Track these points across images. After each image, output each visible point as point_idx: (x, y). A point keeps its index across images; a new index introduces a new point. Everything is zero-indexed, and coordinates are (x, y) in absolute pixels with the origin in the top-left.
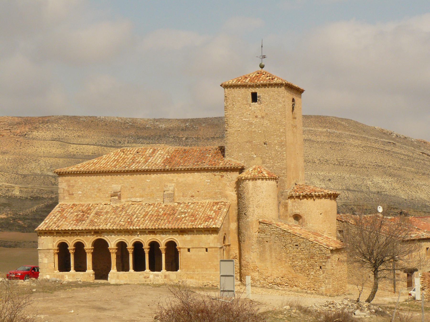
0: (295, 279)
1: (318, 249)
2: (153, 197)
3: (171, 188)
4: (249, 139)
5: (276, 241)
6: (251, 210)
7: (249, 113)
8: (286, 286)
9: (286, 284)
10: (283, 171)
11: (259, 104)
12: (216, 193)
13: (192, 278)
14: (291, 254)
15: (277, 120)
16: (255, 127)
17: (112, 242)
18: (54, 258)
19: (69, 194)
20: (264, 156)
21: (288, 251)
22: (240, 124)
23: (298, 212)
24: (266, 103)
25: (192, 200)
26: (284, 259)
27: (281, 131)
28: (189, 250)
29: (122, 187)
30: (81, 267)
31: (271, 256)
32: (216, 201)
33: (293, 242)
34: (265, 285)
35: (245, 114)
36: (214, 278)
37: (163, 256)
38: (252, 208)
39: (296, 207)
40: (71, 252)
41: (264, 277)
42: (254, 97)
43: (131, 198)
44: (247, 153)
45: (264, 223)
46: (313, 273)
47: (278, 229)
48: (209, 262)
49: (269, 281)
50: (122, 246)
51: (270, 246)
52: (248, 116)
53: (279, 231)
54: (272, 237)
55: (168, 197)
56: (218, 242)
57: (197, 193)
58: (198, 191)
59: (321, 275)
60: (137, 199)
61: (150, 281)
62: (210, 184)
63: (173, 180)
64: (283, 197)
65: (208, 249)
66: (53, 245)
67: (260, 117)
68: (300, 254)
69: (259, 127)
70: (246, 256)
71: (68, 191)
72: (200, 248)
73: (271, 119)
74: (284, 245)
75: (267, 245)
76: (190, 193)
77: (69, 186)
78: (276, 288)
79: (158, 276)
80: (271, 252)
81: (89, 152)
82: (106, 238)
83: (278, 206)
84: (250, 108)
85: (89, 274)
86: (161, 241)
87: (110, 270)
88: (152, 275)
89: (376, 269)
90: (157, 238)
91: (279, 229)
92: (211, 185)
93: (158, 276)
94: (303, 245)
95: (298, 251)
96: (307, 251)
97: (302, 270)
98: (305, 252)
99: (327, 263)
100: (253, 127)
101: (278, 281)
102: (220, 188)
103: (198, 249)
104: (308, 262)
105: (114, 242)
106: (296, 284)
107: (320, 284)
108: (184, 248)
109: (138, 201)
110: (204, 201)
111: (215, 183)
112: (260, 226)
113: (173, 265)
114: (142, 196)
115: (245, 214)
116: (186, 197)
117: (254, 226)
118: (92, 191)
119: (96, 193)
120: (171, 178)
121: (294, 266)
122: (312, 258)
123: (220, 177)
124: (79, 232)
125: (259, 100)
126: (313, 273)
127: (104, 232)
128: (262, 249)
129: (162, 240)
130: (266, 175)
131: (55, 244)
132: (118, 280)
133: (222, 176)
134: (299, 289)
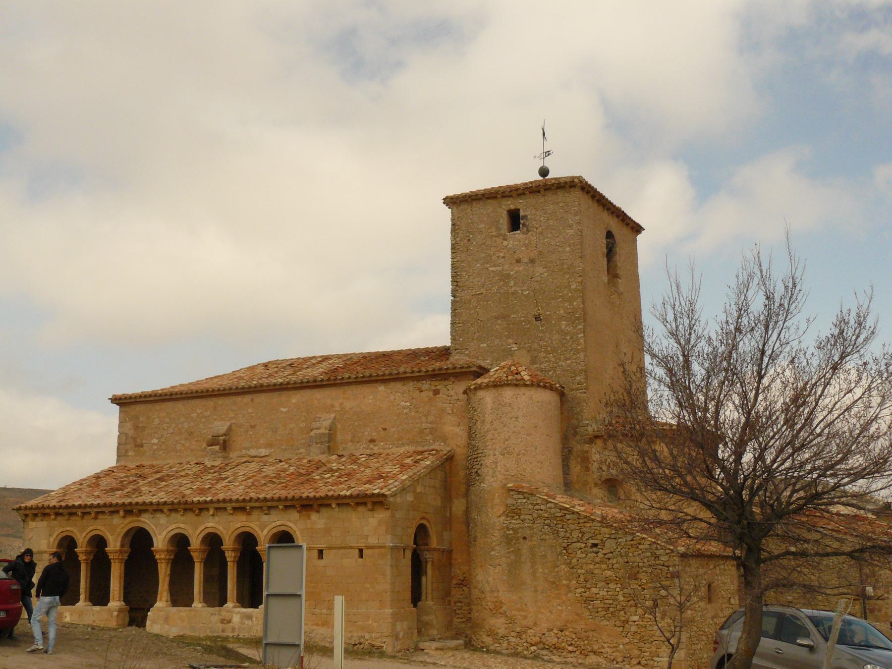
0: (591, 634)
1: (649, 554)
2: (292, 445)
3: (327, 423)
4: (502, 310)
5: (544, 537)
6: (488, 461)
7: (502, 255)
8: (571, 652)
9: (570, 648)
10: (578, 378)
11: (524, 233)
12: (421, 432)
14: (581, 568)
15: (563, 264)
16: (515, 285)
17: (161, 533)
19: (136, 446)
20: (535, 346)
21: (574, 561)
22: (483, 280)
24: (540, 229)
25: (372, 449)
26: (565, 582)
27: (573, 287)
28: (321, 553)
29: (233, 426)
30: (100, 597)
32: (420, 449)
33: (586, 536)
34: (520, 649)
35: (493, 257)
38: (492, 458)
40: (82, 557)
41: (518, 630)
42: (515, 221)
43: (248, 449)
44: (497, 341)
45: (519, 493)
46: (636, 618)
47: (549, 505)
48: (367, 585)
49: (529, 640)
50: (180, 542)
51: (532, 549)
52: (501, 260)
53: (553, 511)
54: (535, 526)
55: (317, 443)
57: (382, 433)
58: (385, 429)
60: (260, 450)
61: (233, 630)
62: (410, 411)
64: (578, 437)
65: (364, 552)
66: (49, 542)
67: (526, 260)
68: (604, 566)
69: (523, 283)
70: (480, 577)
71: (134, 439)
72: (345, 548)
73: (551, 262)
74: (565, 545)
75: (525, 547)
77: (136, 428)
78: (546, 658)
79: (249, 617)
81: (215, 408)
82: (147, 522)
84: (505, 243)
85: (110, 612)
86: (260, 532)
87: (155, 602)
88: (238, 616)
89: (754, 550)
90: (252, 525)
93: (249, 617)
95: (597, 560)
96: (620, 559)
98: (615, 561)
100: (512, 283)
101: (551, 639)
103: (342, 551)
104: (622, 588)
105: (164, 534)
106: (596, 647)
107: (654, 649)
109: (262, 455)
110: (394, 450)
111: (421, 410)
112: (510, 501)
114: (269, 445)
116: (358, 442)
117: (497, 501)
118: (177, 438)
119: (183, 442)
120: (329, 402)
121: (588, 601)
122: (634, 576)
123: (431, 394)
124: (97, 513)
125: (524, 225)
126: (636, 618)
127: (146, 511)
128: (513, 557)
130: (527, 378)
131: (52, 540)
132: (167, 627)
133: (436, 392)
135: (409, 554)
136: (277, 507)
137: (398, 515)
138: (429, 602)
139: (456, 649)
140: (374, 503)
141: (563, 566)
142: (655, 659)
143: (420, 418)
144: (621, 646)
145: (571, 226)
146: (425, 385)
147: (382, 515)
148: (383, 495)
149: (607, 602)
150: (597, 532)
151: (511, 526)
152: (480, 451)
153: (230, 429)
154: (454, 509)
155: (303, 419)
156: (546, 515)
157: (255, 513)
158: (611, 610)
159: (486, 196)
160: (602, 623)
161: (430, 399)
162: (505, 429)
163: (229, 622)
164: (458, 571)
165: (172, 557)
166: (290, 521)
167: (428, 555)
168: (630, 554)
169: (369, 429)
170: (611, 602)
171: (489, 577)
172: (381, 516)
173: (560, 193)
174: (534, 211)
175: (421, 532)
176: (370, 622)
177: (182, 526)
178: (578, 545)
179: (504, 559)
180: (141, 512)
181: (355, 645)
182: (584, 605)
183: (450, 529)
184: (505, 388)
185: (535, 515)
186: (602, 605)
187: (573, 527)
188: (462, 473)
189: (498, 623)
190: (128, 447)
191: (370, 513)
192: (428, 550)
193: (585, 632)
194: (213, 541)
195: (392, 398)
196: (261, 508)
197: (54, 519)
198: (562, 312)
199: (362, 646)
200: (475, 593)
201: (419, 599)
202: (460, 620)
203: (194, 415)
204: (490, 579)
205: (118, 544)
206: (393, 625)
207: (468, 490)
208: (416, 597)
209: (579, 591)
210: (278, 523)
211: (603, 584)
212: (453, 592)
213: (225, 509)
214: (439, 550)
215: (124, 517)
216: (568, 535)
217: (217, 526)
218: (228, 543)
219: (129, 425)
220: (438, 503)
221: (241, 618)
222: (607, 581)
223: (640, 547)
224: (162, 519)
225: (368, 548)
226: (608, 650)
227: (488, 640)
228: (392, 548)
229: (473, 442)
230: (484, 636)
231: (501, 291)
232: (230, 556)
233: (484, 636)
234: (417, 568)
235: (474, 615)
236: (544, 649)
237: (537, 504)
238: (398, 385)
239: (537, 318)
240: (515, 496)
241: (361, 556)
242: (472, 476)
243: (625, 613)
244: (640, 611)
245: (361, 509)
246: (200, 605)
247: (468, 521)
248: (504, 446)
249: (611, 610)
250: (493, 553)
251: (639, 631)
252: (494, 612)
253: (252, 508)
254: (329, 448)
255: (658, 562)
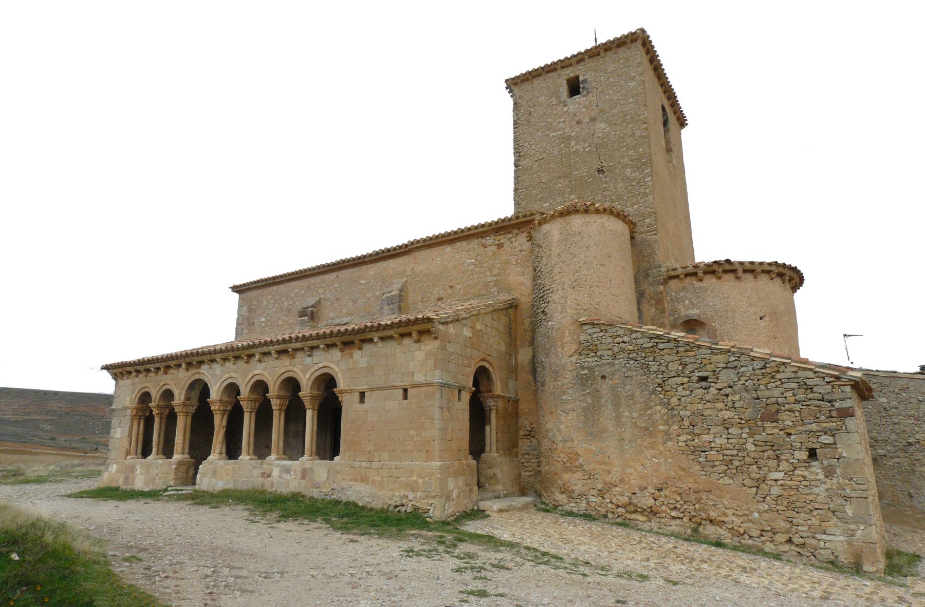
1: (794, 385)
3: (398, 286)
5: (629, 373)
6: (556, 297)
8: (674, 518)
9: (674, 514)
10: (647, 221)
12: (486, 285)
13: (364, 480)
15: (625, 116)
16: (577, 144)
18: (132, 426)
21: (674, 400)
23: (694, 313)
26: (661, 427)
31: (618, 419)
33: (690, 368)
36: (420, 481)
37: (309, 413)
38: (560, 292)
39: (687, 302)
41: (599, 487)
45: (593, 325)
46: (780, 475)
47: (633, 336)
48: (412, 432)
49: (614, 500)
50: (232, 389)
51: (613, 389)
52: (562, 125)
53: (639, 342)
54: (617, 362)
56: (435, 367)
57: (449, 291)
58: (451, 287)
59: (819, 484)
61: (272, 484)
63: (405, 271)
64: (651, 279)
67: (587, 120)
68: (720, 405)
70: (549, 426)
71: (248, 319)
73: (613, 116)
74: (659, 381)
75: (604, 388)
76: (437, 292)
79: (287, 470)
80: (617, 406)
83: (639, 303)
84: (565, 109)
86: (302, 376)
90: (295, 369)
91: (639, 335)
92: (478, 269)
93: (287, 470)
94: (726, 377)
95: (708, 397)
96: (745, 394)
97: (732, 464)
98: (737, 397)
99: (842, 437)
100: (573, 143)
102: (496, 271)
104: (751, 435)
105: (218, 384)
106: (713, 514)
107: (815, 521)
108: (352, 391)
113: (330, 446)
114: (348, 315)
115: (543, 312)
118: (279, 315)
122: (773, 417)
123: (495, 248)
125: (584, 88)
126: (780, 475)
128: (589, 400)
129: (306, 370)
133: (500, 246)
134: (722, 531)
135: (466, 397)
136: (317, 347)
137: (450, 348)
138: (492, 453)
139: (525, 507)
140: (421, 333)
141: (659, 408)
142: (818, 536)
143: (485, 272)
144: (756, 515)
145: (633, 79)
146: (489, 240)
147: (429, 345)
148: (429, 320)
149: (728, 452)
150: (705, 362)
151: (586, 365)
152: (546, 288)
153: (319, 302)
154: (519, 358)
155: (379, 288)
156: (631, 348)
157: (299, 355)
158: (736, 463)
159: (546, 69)
160: (721, 481)
161: (494, 254)
162: (575, 260)
163: (269, 476)
164: (525, 422)
165: (229, 408)
166: (332, 362)
167: (491, 403)
168: (762, 387)
169: (437, 289)
170: (735, 452)
171: (564, 426)
172: (429, 347)
173: (621, 51)
174: (593, 74)
175: (482, 376)
176: (414, 478)
177: (234, 375)
178: (679, 380)
179: (578, 403)
180: (201, 363)
181: (396, 507)
182: (691, 457)
183: (516, 379)
184: (573, 216)
185: (616, 349)
186: (721, 457)
187: (668, 358)
188: (527, 322)
189: (576, 481)
190: (244, 326)
191: (417, 345)
192: (492, 397)
193: (695, 492)
194: (260, 387)
195: (458, 257)
196: (302, 349)
197: (137, 376)
198: (626, 160)
199: (404, 509)
200: (546, 443)
201: (483, 450)
202: (528, 474)
203: (292, 295)
204: (562, 427)
205: (183, 397)
206: (443, 483)
207: (533, 338)
208: (477, 447)
209: (683, 438)
210: (320, 365)
211: (720, 428)
212: (520, 443)
213: (269, 353)
214: (503, 397)
215: (187, 370)
216: (663, 368)
217: (264, 373)
218: (274, 390)
219: (245, 308)
220: (503, 348)
221: (281, 472)
222: (726, 425)
223: (778, 376)
224: (217, 368)
225: (413, 387)
226: (735, 519)
227: (562, 498)
228: (442, 385)
229: (539, 281)
230: (557, 493)
231: (563, 152)
232: (275, 404)
233: (557, 493)
234: (478, 415)
235: (545, 468)
236: (635, 512)
237: (619, 336)
238: (463, 244)
239: (600, 171)
240: (590, 331)
241: (405, 397)
242: (538, 311)
243: (759, 468)
244: (784, 466)
245: (407, 341)
246: (248, 457)
247: (534, 367)
248: (573, 279)
249: (736, 463)
250: (564, 397)
251: (786, 494)
252: (568, 465)
253: (295, 350)
254: (400, 308)
255: (811, 396)
